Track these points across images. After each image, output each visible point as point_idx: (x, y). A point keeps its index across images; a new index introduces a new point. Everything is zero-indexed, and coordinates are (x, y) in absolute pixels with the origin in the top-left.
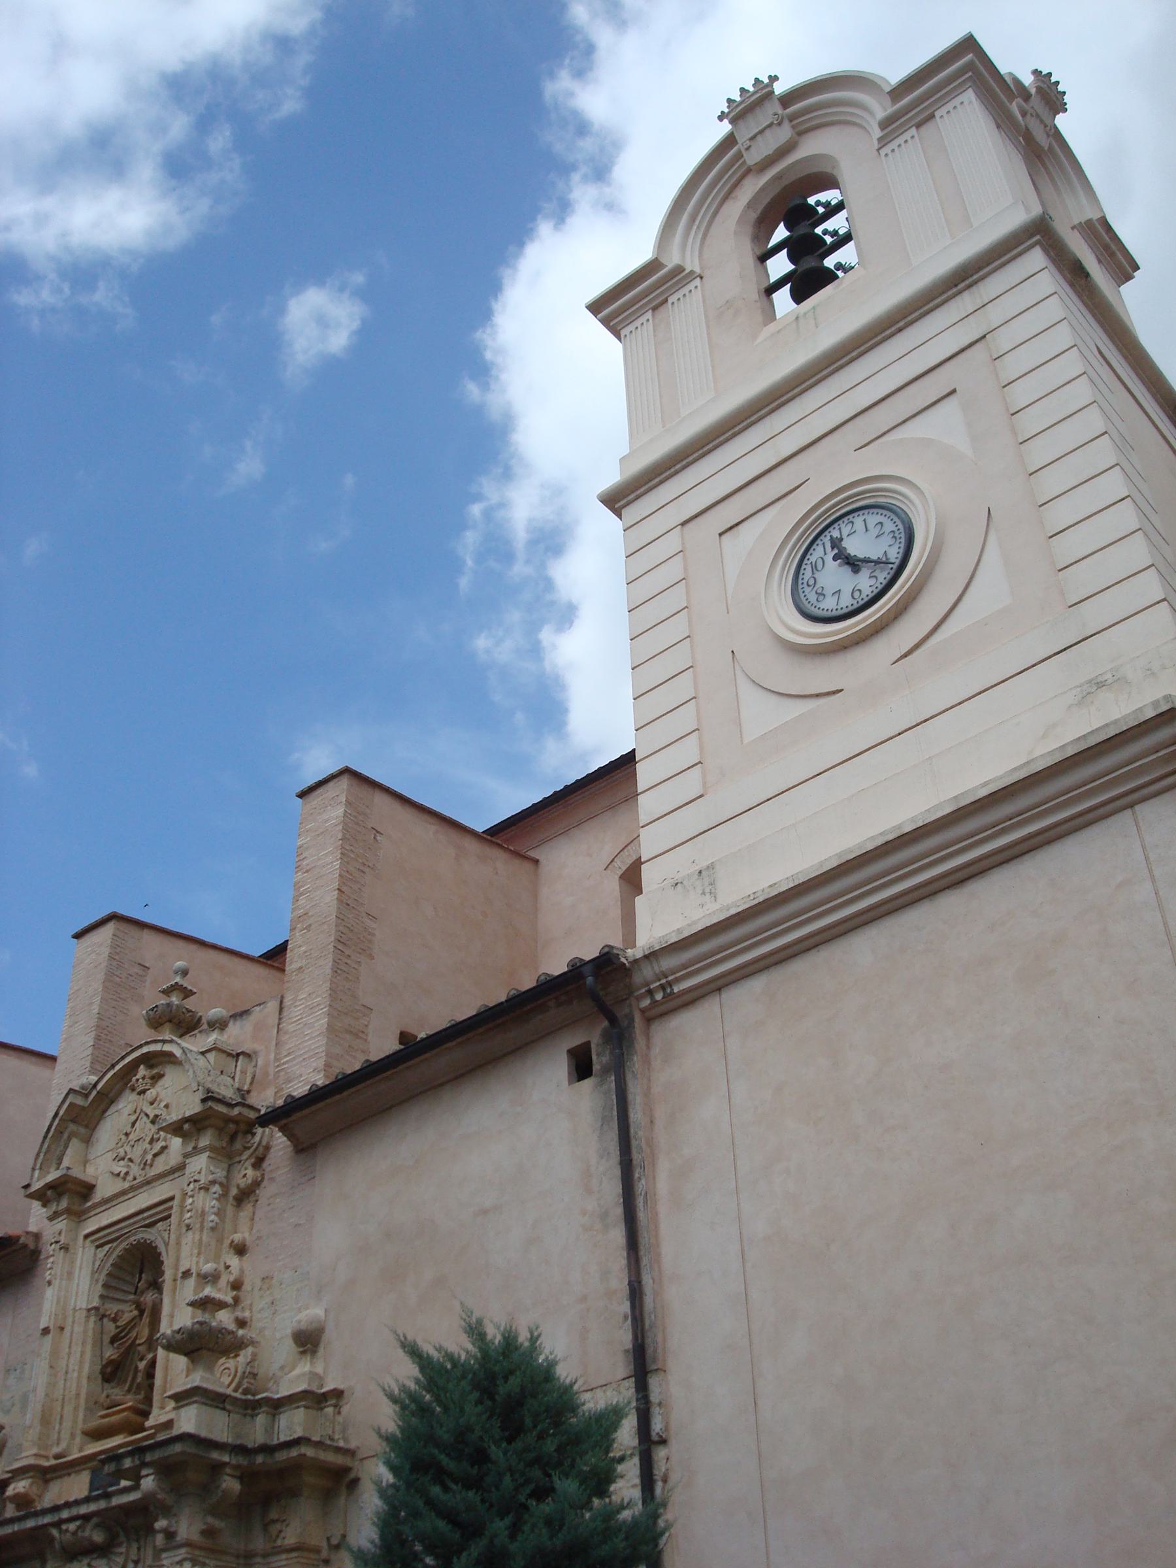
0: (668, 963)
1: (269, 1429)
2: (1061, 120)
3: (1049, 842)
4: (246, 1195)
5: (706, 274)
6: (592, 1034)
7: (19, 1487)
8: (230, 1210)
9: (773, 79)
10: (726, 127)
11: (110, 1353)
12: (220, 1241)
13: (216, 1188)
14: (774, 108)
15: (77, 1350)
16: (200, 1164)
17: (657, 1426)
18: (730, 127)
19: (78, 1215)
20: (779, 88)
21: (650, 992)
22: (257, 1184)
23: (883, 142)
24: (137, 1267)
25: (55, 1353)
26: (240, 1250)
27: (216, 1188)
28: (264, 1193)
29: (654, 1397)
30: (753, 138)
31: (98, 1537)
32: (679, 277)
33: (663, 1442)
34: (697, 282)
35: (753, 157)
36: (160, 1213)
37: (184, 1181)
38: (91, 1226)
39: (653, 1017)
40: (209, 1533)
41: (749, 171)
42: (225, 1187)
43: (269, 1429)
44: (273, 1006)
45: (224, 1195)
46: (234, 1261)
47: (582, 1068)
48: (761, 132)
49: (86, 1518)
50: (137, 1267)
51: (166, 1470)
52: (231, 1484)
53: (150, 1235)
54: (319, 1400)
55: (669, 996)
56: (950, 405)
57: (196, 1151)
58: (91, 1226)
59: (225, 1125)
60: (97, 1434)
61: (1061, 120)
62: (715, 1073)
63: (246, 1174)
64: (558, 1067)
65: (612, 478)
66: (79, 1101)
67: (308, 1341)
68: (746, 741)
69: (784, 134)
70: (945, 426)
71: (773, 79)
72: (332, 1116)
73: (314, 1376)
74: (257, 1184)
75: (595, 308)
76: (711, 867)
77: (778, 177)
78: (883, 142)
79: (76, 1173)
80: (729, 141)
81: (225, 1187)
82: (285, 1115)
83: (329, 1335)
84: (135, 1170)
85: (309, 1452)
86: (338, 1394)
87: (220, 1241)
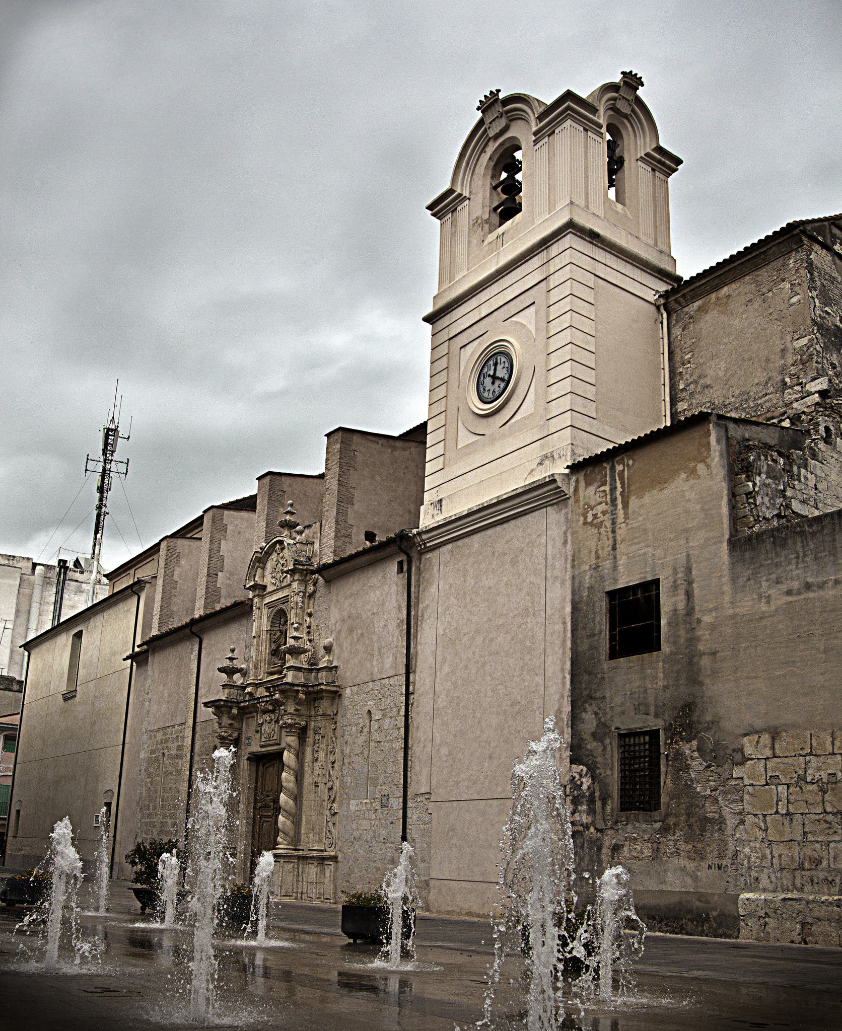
0: (424, 537)
1: (316, 678)
2: (640, 92)
3: (525, 514)
4: (311, 596)
5: (472, 197)
6: (404, 558)
7: (249, 689)
8: (306, 601)
9: (498, 91)
10: (479, 114)
11: (274, 647)
12: (303, 612)
13: (301, 594)
14: (499, 108)
15: (264, 644)
16: (295, 585)
17: (411, 689)
18: (481, 115)
19: (262, 597)
20: (501, 96)
21: (420, 545)
22: (314, 592)
23: (536, 142)
24: (280, 616)
25: (258, 645)
26: (310, 615)
27: (301, 594)
28: (317, 595)
29: (411, 680)
30: (491, 123)
31: (271, 708)
32: (461, 198)
33: (413, 693)
34: (467, 202)
35: (491, 133)
36: (285, 600)
37: (291, 590)
38: (267, 600)
39: (421, 554)
40: (296, 710)
41: (490, 138)
42: (304, 593)
43: (316, 678)
44: (318, 524)
45: (305, 595)
46: (308, 619)
47: (400, 570)
48: (494, 120)
49: (267, 702)
50: (280, 616)
51: (282, 692)
52: (302, 696)
53: (283, 607)
54: (330, 669)
55: (425, 547)
56: (533, 308)
57: (294, 581)
58: (267, 600)
59: (303, 571)
60: (271, 674)
61: (640, 92)
62: (443, 573)
63: (311, 588)
64: (394, 567)
65: (429, 310)
66: (259, 555)
67: (328, 649)
68: (459, 447)
69: (503, 122)
70: (528, 318)
71: (498, 91)
72: (337, 571)
73: (330, 662)
74: (314, 592)
75: (430, 208)
76: (441, 500)
77: (501, 144)
78: (536, 142)
79: (260, 582)
80: (481, 122)
81: (304, 593)
82: (323, 569)
83: (334, 647)
84: (278, 583)
85: (323, 687)
86: (336, 667)
87: (303, 612)
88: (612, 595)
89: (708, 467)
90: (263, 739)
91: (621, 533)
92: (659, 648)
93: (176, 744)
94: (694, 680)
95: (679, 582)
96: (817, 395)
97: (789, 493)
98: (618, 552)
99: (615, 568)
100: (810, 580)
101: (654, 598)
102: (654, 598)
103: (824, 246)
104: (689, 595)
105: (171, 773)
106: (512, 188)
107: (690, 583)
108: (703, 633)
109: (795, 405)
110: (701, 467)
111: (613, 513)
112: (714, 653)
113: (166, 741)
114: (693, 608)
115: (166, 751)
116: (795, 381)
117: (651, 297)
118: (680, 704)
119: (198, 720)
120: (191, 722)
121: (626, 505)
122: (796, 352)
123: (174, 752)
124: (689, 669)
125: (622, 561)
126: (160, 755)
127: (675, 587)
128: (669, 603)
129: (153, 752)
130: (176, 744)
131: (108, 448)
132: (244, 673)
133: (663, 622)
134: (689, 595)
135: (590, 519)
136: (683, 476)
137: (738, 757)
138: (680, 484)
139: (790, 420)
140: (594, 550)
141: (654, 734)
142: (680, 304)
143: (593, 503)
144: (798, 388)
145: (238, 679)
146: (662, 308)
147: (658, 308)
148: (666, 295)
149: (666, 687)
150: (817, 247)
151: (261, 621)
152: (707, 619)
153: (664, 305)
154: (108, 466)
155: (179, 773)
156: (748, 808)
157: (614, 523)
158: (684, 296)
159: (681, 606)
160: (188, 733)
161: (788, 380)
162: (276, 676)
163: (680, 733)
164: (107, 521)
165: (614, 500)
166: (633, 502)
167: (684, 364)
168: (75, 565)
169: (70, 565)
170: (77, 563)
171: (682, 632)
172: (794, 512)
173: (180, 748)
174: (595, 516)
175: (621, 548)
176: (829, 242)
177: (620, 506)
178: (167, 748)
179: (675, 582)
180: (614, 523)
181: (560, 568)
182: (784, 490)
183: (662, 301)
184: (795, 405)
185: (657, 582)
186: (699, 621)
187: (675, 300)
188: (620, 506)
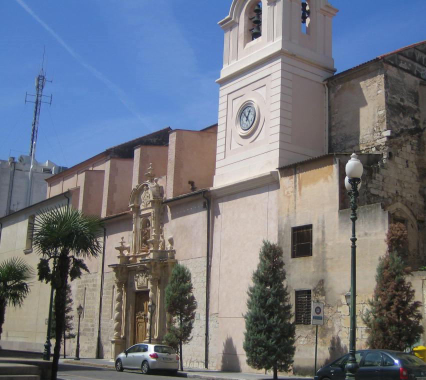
56: (265, 87)
88: (295, 229)
89: (332, 177)
90: (139, 284)
91: (298, 201)
92: (311, 255)
93: (92, 283)
94: (324, 270)
95: (320, 226)
96: (386, 138)
97: (369, 186)
98: (297, 210)
99: (295, 217)
100: (367, 231)
101: (310, 232)
102: (310, 232)
103: (395, 65)
104: (323, 233)
105: (90, 299)
106: (258, 23)
107: (324, 227)
108: (328, 250)
109: (378, 141)
110: (329, 178)
111: (295, 192)
112: (332, 259)
113: (87, 281)
114: (325, 239)
115: (86, 286)
116: (378, 130)
117: (321, 80)
118: (319, 280)
119: (105, 271)
120: (100, 272)
121: (300, 189)
122: (379, 117)
123: (91, 287)
124: (322, 265)
125: (298, 215)
126: (84, 289)
127: (318, 229)
128: (316, 236)
129: (79, 287)
130: (92, 283)
131: (40, 87)
132: (128, 249)
133: (313, 244)
134: (323, 233)
135: (286, 193)
136: (322, 180)
137: (339, 304)
138: (321, 183)
139: (376, 148)
140: (287, 209)
141: (309, 292)
142: (334, 85)
143: (200, 335)
144: (379, 133)
145: (126, 253)
146: (326, 85)
147: (324, 85)
148: (328, 80)
149: (314, 272)
150: (390, 67)
151: (137, 224)
152: (330, 244)
153: (327, 84)
154: (39, 98)
155: (94, 298)
156: (343, 325)
157: (295, 197)
158: (335, 81)
159: (320, 237)
160: (99, 278)
161: (375, 129)
162: (145, 253)
163: (319, 292)
164: (40, 135)
165: (295, 186)
166: (303, 189)
167: (334, 114)
168: (20, 161)
169: (17, 160)
170: (21, 159)
171: (320, 249)
172: (371, 194)
173: (94, 285)
174: (288, 193)
175: (298, 208)
176: (396, 63)
177: (298, 189)
178: (88, 285)
179: (318, 226)
180: (295, 197)
181: (274, 214)
182: (367, 185)
183: (325, 83)
184: (378, 141)
185: (310, 226)
186: (327, 244)
187: (332, 83)
188: (298, 189)
